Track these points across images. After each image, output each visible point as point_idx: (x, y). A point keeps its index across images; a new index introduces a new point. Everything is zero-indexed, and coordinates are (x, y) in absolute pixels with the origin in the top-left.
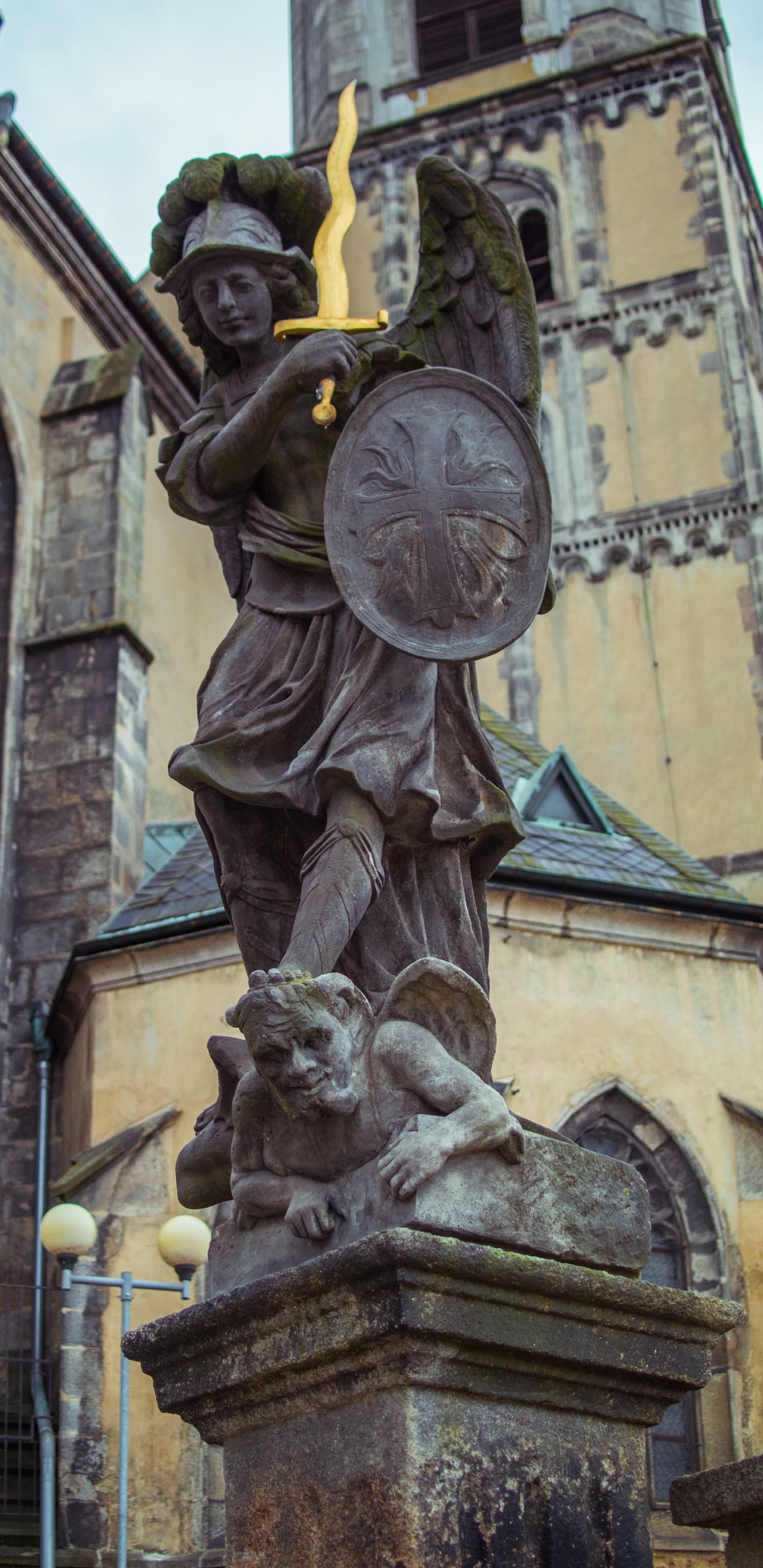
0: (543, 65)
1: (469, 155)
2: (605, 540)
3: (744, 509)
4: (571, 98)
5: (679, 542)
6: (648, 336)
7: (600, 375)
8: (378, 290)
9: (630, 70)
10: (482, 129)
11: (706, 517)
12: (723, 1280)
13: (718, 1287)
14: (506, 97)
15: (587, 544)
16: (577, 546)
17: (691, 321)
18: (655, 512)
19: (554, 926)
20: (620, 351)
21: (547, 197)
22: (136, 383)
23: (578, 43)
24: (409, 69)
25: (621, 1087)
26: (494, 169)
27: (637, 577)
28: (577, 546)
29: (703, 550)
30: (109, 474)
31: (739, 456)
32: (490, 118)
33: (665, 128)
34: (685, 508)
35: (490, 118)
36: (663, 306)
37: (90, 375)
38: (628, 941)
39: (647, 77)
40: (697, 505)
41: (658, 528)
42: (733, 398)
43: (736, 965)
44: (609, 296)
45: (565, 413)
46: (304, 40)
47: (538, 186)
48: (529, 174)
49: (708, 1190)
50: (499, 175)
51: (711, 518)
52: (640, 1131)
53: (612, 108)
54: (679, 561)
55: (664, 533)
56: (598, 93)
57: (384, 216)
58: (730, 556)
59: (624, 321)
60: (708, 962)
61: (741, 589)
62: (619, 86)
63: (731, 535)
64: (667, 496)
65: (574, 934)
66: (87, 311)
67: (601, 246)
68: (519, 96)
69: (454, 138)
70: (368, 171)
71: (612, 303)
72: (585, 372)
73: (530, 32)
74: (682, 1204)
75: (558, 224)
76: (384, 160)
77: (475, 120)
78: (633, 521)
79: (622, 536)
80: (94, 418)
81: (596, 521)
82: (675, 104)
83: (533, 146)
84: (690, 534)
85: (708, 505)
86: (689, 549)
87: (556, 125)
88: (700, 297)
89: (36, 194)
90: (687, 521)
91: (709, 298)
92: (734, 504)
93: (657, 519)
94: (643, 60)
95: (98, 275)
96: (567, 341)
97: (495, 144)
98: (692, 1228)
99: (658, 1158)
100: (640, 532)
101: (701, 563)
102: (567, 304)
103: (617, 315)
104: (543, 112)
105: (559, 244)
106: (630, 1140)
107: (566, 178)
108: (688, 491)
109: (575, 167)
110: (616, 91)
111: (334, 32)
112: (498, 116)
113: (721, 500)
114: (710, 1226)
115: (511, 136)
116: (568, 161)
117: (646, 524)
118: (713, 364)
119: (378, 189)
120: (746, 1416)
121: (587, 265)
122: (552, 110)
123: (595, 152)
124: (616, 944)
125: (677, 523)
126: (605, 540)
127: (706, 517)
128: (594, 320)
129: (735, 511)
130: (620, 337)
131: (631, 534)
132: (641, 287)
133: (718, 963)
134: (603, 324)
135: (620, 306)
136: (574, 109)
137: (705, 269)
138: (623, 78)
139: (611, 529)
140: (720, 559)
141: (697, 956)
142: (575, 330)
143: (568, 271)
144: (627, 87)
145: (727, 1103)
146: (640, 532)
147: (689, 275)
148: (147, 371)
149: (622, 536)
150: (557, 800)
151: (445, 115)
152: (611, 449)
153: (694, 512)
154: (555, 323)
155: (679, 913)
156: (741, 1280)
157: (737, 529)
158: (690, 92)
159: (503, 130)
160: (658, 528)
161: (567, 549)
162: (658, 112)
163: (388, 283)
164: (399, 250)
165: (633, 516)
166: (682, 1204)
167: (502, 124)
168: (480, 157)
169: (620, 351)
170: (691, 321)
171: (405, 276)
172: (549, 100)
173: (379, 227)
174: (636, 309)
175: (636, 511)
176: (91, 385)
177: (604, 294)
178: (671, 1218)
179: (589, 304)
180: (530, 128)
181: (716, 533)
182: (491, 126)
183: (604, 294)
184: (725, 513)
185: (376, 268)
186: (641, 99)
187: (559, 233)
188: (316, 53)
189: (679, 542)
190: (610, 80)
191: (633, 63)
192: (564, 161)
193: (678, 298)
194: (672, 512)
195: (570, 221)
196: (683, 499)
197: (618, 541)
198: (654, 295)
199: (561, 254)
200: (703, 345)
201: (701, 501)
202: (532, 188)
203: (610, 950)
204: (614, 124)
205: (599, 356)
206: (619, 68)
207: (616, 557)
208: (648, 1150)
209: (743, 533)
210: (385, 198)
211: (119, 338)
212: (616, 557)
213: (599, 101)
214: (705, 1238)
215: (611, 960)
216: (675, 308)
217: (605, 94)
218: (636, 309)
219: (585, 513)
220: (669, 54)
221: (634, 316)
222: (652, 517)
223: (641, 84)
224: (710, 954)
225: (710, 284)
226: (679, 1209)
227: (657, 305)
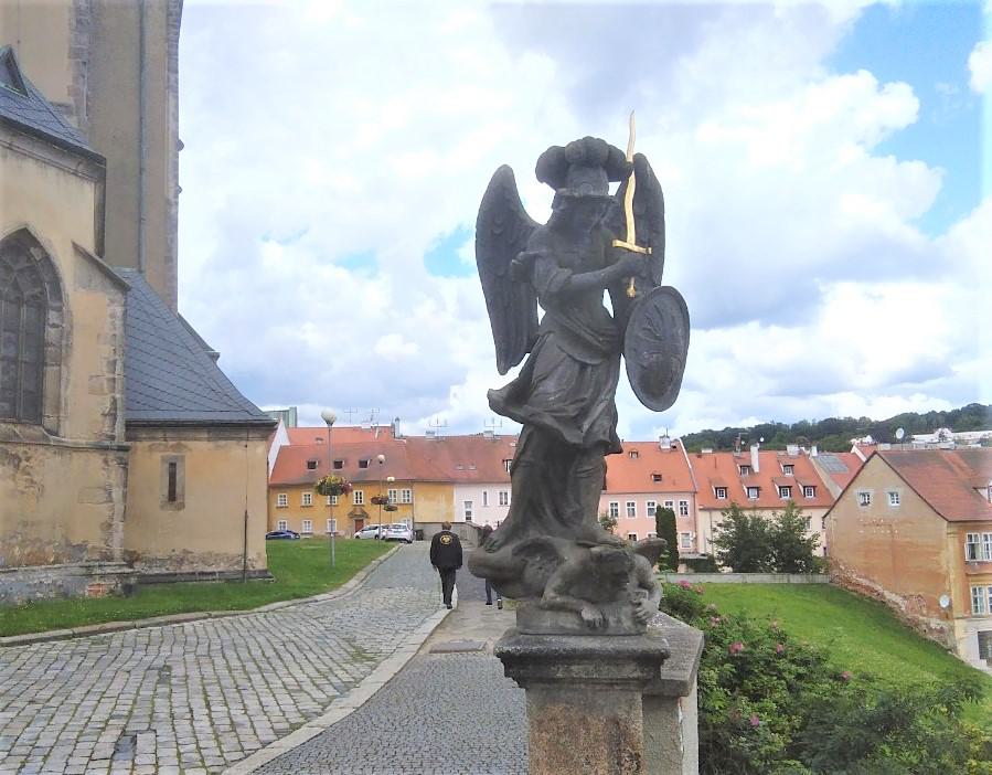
52: (32, 250)
60: (74, 177)
74: (47, 287)
114: (60, 299)
133: (78, 179)
152: (320, 442)
156: (72, 327)
166: (47, 287)
203: (30, 160)
214: (57, 304)
215: (30, 166)
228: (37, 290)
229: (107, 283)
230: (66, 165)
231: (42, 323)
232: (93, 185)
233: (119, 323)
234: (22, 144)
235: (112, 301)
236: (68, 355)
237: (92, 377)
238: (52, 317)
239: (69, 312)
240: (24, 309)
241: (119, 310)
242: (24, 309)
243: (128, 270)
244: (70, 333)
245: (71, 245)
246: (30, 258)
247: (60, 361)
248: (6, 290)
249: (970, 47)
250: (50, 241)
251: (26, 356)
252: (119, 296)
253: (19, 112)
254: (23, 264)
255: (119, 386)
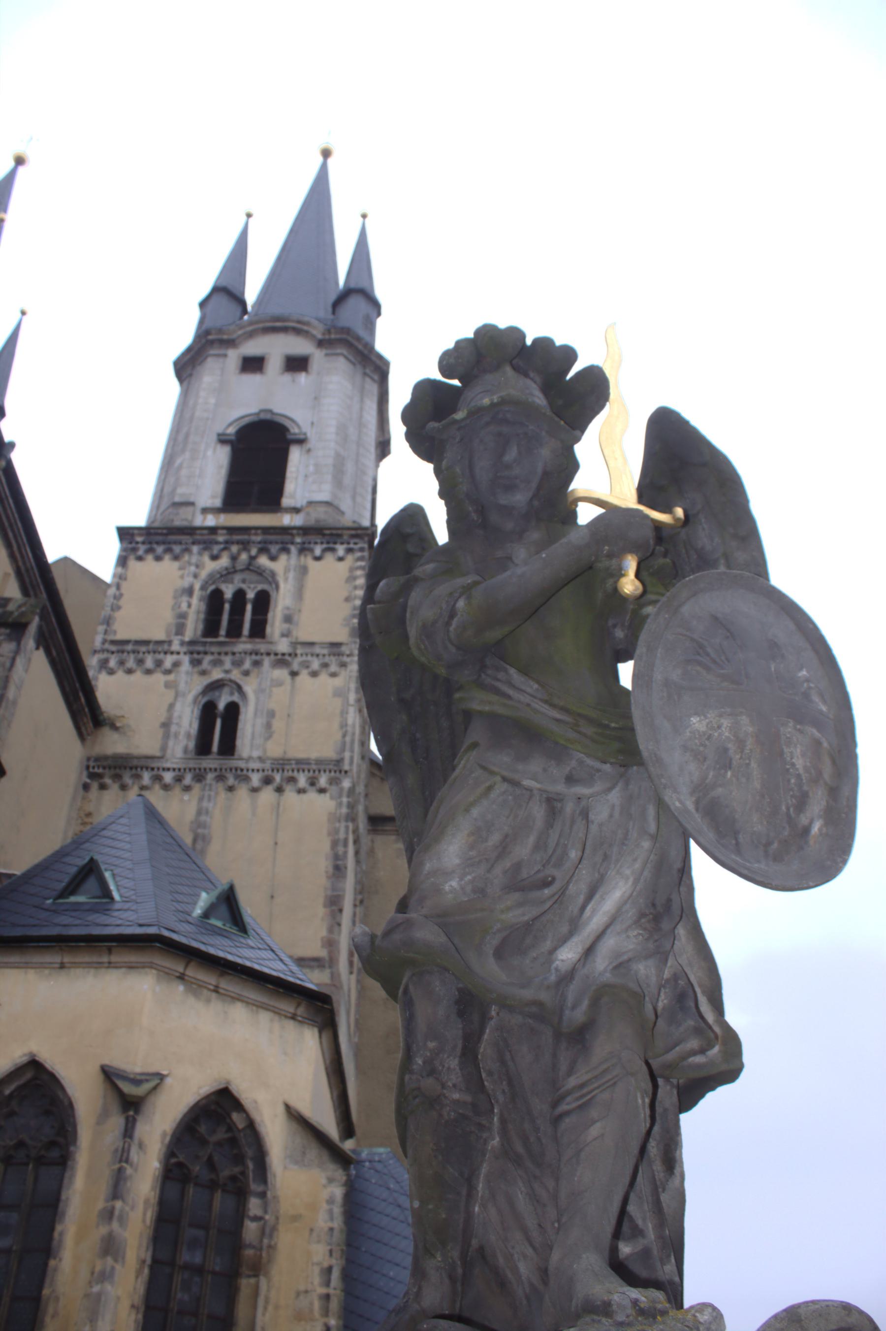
0: (287, 520)
1: (239, 553)
2: (263, 770)
3: (340, 772)
4: (298, 540)
5: (302, 781)
6: (310, 670)
7: (280, 684)
8: (173, 609)
9: (331, 535)
10: (248, 542)
11: (319, 771)
12: (267, 1217)
13: (262, 1222)
14: (266, 530)
15: (253, 770)
16: (248, 770)
17: (333, 668)
18: (293, 762)
19: (210, 984)
20: (294, 674)
21: (274, 586)
22: (37, 619)
23: (308, 514)
24: (218, 502)
25: (230, 1088)
26: (250, 564)
27: (276, 794)
28: (248, 770)
29: (314, 788)
30: (8, 664)
31: (344, 744)
32: (254, 538)
33: (343, 568)
34: (309, 764)
35: (254, 538)
36: (321, 657)
37: (11, 607)
38: (250, 1001)
39: (339, 541)
40: (316, 764)
41: (293, 771)
42: (347, 713)
43: (306, 1026)
44: (295, 644)
45: (257, 699)
46: (167, 472)
47: (270, 579)
48: (267, 572)
49: (268, 1159)
50: (251, 568)
51: (322, 772)
53: (318, 551)
54: (301, 791)
55: (295, 774)
56: (312, 541)
57: (187, 572)
58: (328, 795)
59: (299, 659)
60: (292, 1022)
61: (330, 814)
62: (324, 541)
63: (331, 784)
64: (301, 755)
65: (221, 991)
66: (19, 573)
67: (296, 618)
68: (272, 531)
69: (233, 543)
70: (184, 547)
71: (295, 649)
72: (272, 680)
73: (286, 502)
75: (276, 601)
76: (194, 543)
77: (246, 537)
78: (281, 764)
79: (273, 770)
80: (8, 631)
81: (260, 759)
82: (350, 558)
83: (273, 558)
84: (310, 778)
85: (321, 765)
86: (328, 786)
87: (286, 550)
88: (341, 657)
89: (11, 501)
90: (309, 771)
91: (345, 659)
92: (335, 768)
93: (294, 766)
94: (339, 532)
95: (30, 555)
96: (267, 662)
97: (254, 552)
98: (254, 1181)
99: (242, 1134)
100: (283, 770)
101: (312, 795)
102: (271, 643)
103: (296, 655)
104: (282, 543)
105: (274, 611)
106: (228, 1121)
107: (286, 579)
108: (314, 755)
109: (291, 575)
110: (322, 543)
111: (184, 472)
112: (259, 538)
113: (329, 764)
115: (263, 550)
116: (289, 570)
117: (288, 767)
118: (339, 693)
119: (186, 557)
120: (265, 1308)
121: (286, 626)
122: (287, 543)
123: (304, 570)
124: (242, 1001)
125: (303, 771)
126: (263, 770)
127: (319, 771)
128: (283, 654)
129: (335, 772)
130: (295, 666)
131: (278, 771)
132: (312, 644)
134: (287, 657)
135: (299, 651)
136: (299, 546)
137: (347, 644)
138: (327, 538)
139: (268, 765)
140: (322, 795)
141: (286, 1017)
142: (272, 657)
143: (275, 625)
144: (328, 543)
145: (288, 1108)
146: (283, 770)
147: (337, 645)
148: (43, 617)
149: (273, 770)
150: (223, 909)
151: (231, 530)
152: (278, 724)
153: (314, 767)
154: (262, 651)
155: (281, 990)
156: (277, 1218)
157: (334, 781)
158: (359, 554)
159: (260, 546)
160: (293, 771)
161: (242, 770)
162: (341, 559)
163: (179, 607)
164: (190, 591)
165: (281, 762)
166: (251, 1165)
167: (260, 543)
168: (244, 556)
169: (294, 674)
170: (333, 668)
171: (189, 606)
172: (287, 538)
173: (182, 577)
174: (307, 655)
175: (283, 759)
176: (12, 613)
177: (292, 643)
178: (243, 1173)
179: (283, 646)
180: (274, 549)
181: (323, 781)
182: (254, 542)
183: (292, 643)
184: (330, 771)
185: (175, 597)
186: (333, 550)
187: (276, 606)
188: (171, 480)
189: (302, 781)
190: (320, 536)
191: (334, 532)
192: (287, 570)
193: (329, 655)
194: (302, 764)
195: (282, 601)
196: (308, 759)
197: (270, 772)
198: (317, 650)
199: (274, 616)
200: (338, 682)
201: (319, 762)
202: (267, 579)
203: (239, 1005)
204: (318, 559)
205: (281, 673)
206: (327, 532)
207: (267, 781)
208: (237, 1128)
209: (337, 784)
210: (189, 563)
211: (32, 593)
212: (267, 781)
213: (312, 546)
214: (260, 1188)
215: (239, 1012)
216: (327, 659)
217: (316, 543)
218: (307, 655)
219: (256, 754)
220: (353, 532)
221: (304, 658)
222: (291, 764)
223: (335, 543)
224: (293, 1017)
225: (348, 652)
226: (248, 1168)
227: (318, 655)
228: (237, 1170)
229: (325, 1155)
230: (126, 960)
231: (240, 1214)
232: (316, 1030)
233: (337, 1210)
234: (228, 985)
235: (331, 1180)
236: (270, 1261)
237: (298, 1294)
238: (254, 1206)
239: (275, 1197)
240: (218, 1196)
241: (338, 1192)
242: (218, 1196)
243: (381, 1150)
244: (274, 1229)
245: (281, 1109)
246: (231, 1127)
247: (258, 1269)
248: (198, 1168)
249: (460, 381)
250: (256, 1102)
251: (217, 1264)
252: (340, 1175)
253: (234, 950)
254: (221, 1134)
255: (334, 1305)
